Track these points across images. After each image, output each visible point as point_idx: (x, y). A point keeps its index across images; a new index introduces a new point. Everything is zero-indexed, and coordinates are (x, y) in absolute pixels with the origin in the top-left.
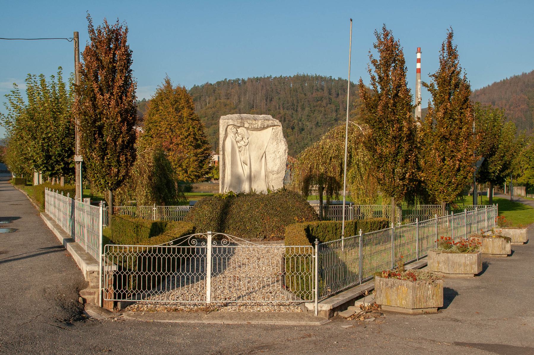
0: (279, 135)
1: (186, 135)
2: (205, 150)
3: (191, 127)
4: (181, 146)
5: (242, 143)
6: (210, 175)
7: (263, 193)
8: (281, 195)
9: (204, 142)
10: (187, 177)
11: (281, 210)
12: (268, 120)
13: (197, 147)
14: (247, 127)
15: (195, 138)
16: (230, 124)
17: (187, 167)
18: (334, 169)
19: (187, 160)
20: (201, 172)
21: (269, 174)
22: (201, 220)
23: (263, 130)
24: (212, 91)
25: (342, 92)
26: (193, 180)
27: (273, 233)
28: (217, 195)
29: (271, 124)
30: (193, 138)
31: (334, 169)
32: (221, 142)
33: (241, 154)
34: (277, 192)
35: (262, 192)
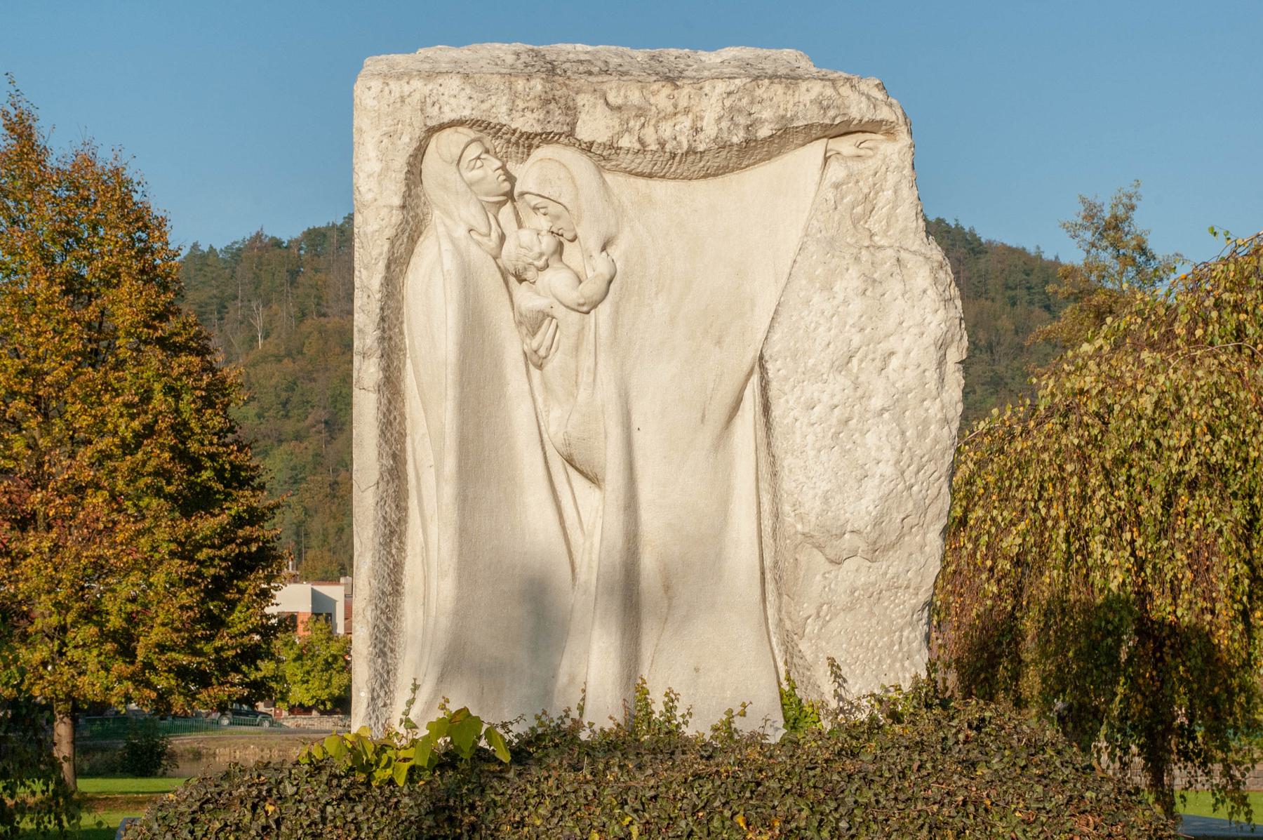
0: (882, 212)
1: (129, 435)
2: (239, 522)
3: (157, 386)
4: (97, 500)
5: (557, 281)
6: (267, 667)
7: (744, 726)
8: (921, 746)
9: (237, 478)
12: (792, 79)
14: (602, 137)
15: (181, 455)
16: (448, 116)
17: (130, 618)
18: (1199, 565)
19: (135, 577)
20: (218, 650)
21: (802, 558)
23: (738, 168)
29: (814, 116)
30: (172, 449)
31: (1199, 565)
33: (545, 384)
34: (872, 719)
35: (738, 723)
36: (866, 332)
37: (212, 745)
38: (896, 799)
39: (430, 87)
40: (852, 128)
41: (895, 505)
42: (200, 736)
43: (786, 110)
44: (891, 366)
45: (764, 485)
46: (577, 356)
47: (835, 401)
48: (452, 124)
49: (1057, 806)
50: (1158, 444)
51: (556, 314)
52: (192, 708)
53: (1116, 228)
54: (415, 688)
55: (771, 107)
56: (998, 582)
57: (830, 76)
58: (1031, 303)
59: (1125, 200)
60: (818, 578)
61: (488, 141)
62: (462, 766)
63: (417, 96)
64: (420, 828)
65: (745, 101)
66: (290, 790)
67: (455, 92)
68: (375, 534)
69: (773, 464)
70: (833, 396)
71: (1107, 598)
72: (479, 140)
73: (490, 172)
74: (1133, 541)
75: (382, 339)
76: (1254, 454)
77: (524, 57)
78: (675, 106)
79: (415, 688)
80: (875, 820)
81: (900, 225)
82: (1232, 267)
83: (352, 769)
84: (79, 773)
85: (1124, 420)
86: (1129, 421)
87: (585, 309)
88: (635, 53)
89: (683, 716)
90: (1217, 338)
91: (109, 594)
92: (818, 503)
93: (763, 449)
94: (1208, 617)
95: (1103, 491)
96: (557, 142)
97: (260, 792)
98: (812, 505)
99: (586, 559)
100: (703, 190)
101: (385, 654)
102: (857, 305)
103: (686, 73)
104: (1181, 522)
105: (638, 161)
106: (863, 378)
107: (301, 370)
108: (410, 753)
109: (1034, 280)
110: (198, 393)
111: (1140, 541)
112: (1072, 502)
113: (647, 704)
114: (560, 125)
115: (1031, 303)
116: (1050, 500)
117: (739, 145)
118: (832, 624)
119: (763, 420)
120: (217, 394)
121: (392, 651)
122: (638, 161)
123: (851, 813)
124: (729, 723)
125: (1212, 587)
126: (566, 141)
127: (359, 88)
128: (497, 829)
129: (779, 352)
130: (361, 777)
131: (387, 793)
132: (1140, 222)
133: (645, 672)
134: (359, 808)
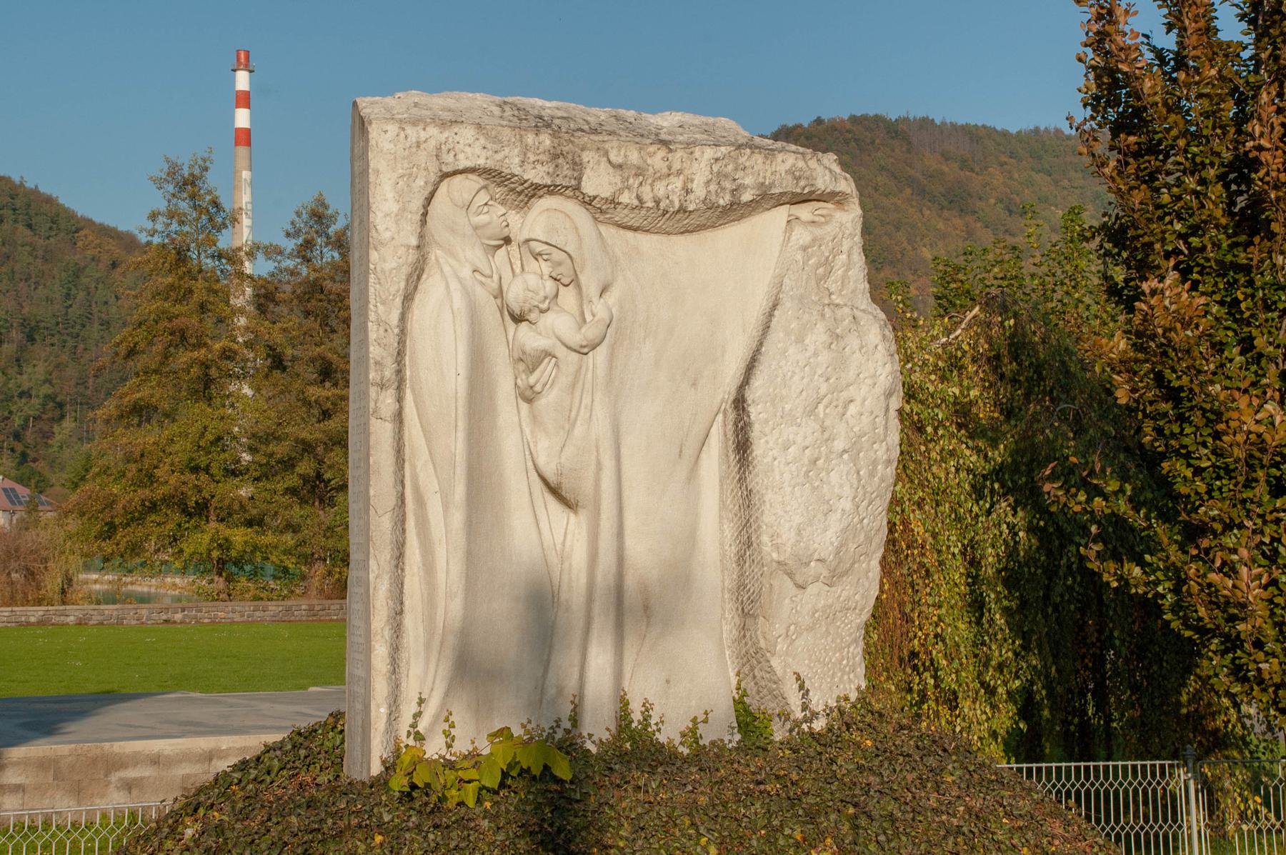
14: (606, 193)
16: (463, 163)
21: (776, 583)
29: (789, 185)
35: (702, 729)
36: (831, 381)
39: (446, 134)
40: (813, 197)
41: (851, 537)
43: (765, 178)
44: (849, 413)
46: (572, 393)
47: (807, 443)
51: (558, 354)
55: (753, 174)
59: (200, 162)
60: (787, 601)
63: (432, 143)
65: (730, 167)
67: (471, 142)
72: (485, 187)
73: (495, 218)
79: (421, 701)
89: (657, 724)
92: (793, 534)
96: (561, 194)
100: (682, 245)
102: (824, 358)
105: (632, 216)
106: (827, 423)
109: (18, 203)
114: (567, 179)
115: (16, 221)
118: (797, 643)
122: (632, 216)
126: (572, 194)
129: (760, 397)
133: (626, 685)
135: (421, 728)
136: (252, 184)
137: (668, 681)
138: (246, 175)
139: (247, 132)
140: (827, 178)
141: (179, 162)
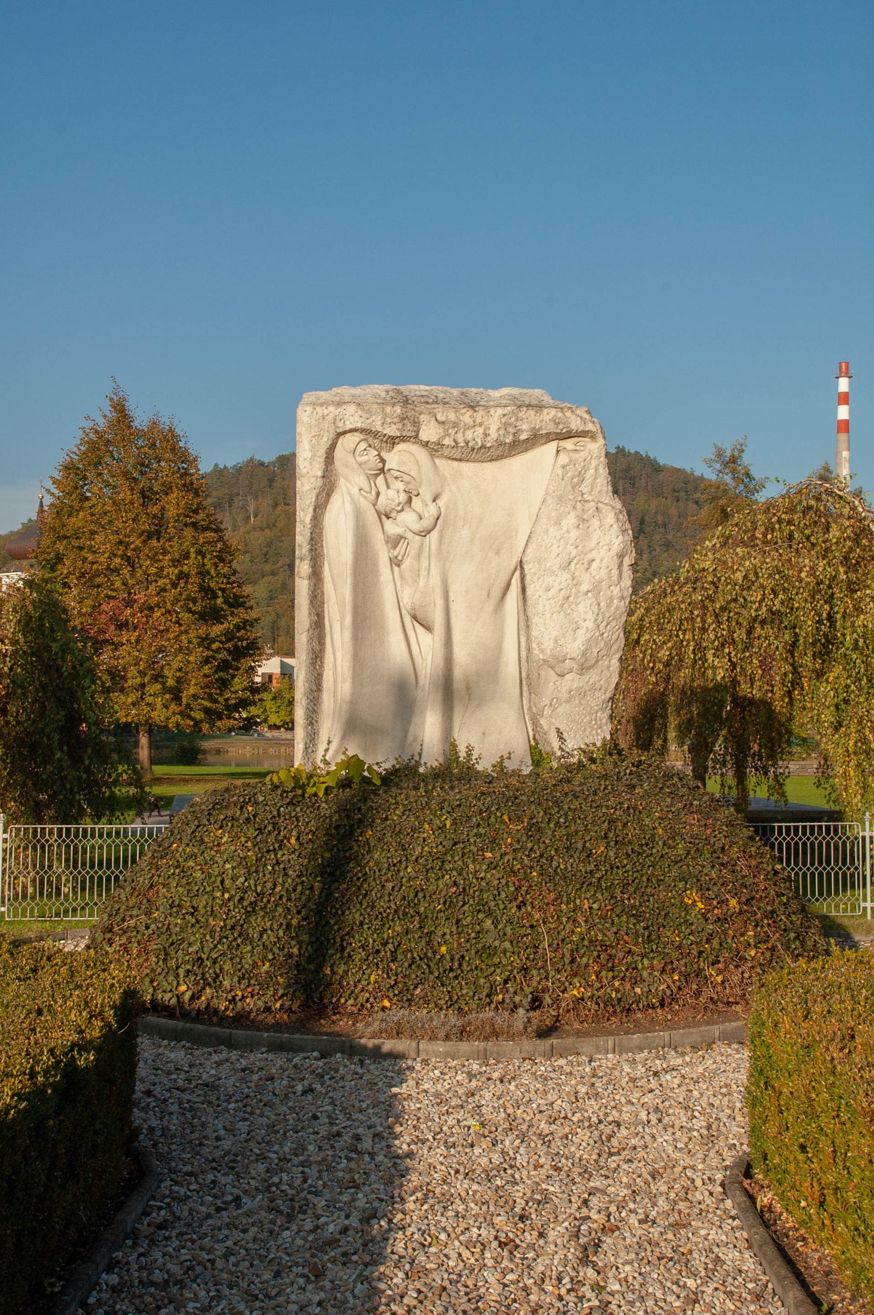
0: (588, 481)
2: (238, 628)
3: (192, 550)
5: (408, 518)
6: (254, 710)
7: (510, 765)
8: (606, 777)
10: (181, 713)
11: (611, 853)
12: (539, 407)
13: (212, 615)
14: (434, 438)
16: (349, 426)
17: (179, 680)
18: (765, 666)
20: (227, 700)
21: (543, 673)
22: (195, 909)
23: (509, 456)
24: (265, 481)
25: (627, 486)
26: (197, 723)
27: (576, 981)
28: (283, 775)
29: (551, 428)
31: (765, 666)
32: (302, 539)
33: (402, 576)
34: (580, 761)
35: (506, 763)
37: (226, 746)
38: (591, 806)
39: (339, 410)
40: (572, 435)
42: (220, 741)
45: (522, 632)
47: (561, 587)
48: (351, 431)
49: (678, 810)
50: (745, 599)
52: (213, 731)
53: (734, 462)
54: (329, 742)
56: (656, 675)
57: (561, 406)
58: (687, 500)
59: (738, 447)
60: (551, 684)
61: (371, 440)
62: (354, 786)
63: (331, 416)
64: (331, 820)
65: (513, 419)
66: (261, 799)
68: (307, 658)
69: (527, 621)
70: (560, 583)
71: (715, 684)
74: (730, 653)
75: (311, 550)
76: (796, 605)
77: (391, 394)
78: (474, 422)
79: (329, 742)
80: (579, 818)
81: (598, 489)
82: (787, 500)
83: (294, 787)
84: (154, 761)
85: (727, 586)
86: (729, 587)
87: (423, 534)
88: (452, 391)
90: (779, 540)
91: (167, 667)
93: (522, 612)
94: (770, 695)
95: (714, 626)
97: (245, 799)
98: (548, 644)
99: (424, 672)
100: (490, 469)
101: (313, 724)
102: (574, 533)
103: (481, 403)
104: (756, 642)
106: (577, 574)
107: (275, 536)
108: (326, 779)
109: (689, 487)
110: (215, 554)
111: (733, 654)
112: (697, 632)
113: (457, 753)
115: (687, 500)
116: (685, 630)
117: (510, 444)
118: (559, 710)
119: (522, 596)
120: (224, 555)
121: (317, 722)
123: (566, 814)
124: (501, 763)
125: (772, 678)
127: (299, 411)
128: (373, 822)
130: (300, 792)
131: (313, 801)
132: (746, 459)
133: (455, 735)
134: (298, 809)
135: (327, 758)
136: (850, 461)
137: (484, 734)
138: (845, 454)
139: (846, 422)
140: (578, 422)
141: (724, 448)
